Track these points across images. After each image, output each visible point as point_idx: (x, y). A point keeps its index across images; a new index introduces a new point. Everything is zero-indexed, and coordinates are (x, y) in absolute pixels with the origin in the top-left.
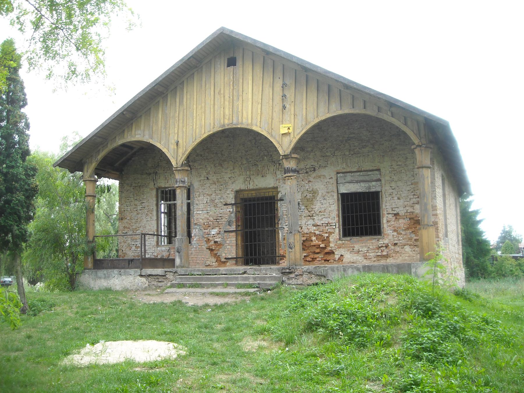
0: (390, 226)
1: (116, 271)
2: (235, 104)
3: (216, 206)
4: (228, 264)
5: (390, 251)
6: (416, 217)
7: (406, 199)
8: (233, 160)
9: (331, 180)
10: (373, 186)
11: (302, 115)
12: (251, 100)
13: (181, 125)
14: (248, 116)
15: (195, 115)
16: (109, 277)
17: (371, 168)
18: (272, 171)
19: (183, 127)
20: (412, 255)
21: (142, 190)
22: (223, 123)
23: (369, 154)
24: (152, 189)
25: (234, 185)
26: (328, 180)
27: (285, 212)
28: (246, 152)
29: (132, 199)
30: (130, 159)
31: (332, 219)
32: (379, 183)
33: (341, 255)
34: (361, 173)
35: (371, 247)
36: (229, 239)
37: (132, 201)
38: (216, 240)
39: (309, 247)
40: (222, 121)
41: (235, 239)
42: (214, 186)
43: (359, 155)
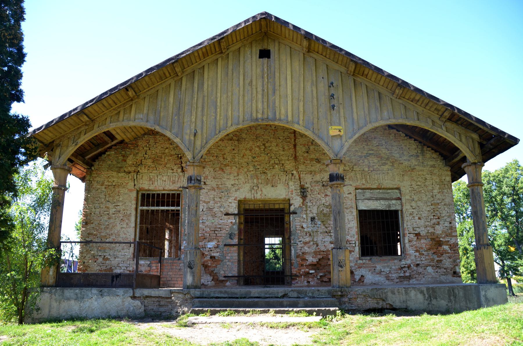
0: (412, 246)
1: (95, 291)
2: (271, 98)
3: (214, 216)
4: (228, 284)
5: (412, 272)
6: (437, 237)
7: (426, 219)
8: (237, 166)
9: (349, 195)
10: (393, 204)
11: (353, 119)
12: (290, 96)
13: (199, 113)
14: (287, 112)
15: (218, 104)
16: (83, 298)
17: (391, 186)
18: (284, 181)
19: (203, 115)
20: (435, 276)
21: (117, 190)
22: (255, 117)
23: (389, 172)
24: (131, 191)
25: (238, 193)
26: (347, 195)
27: (298, 226)
28: (254, 158)
29: (103, 200)
30: (104, 153)
31: (351, 237)
32: (399, 202)
33: (362, 276)
34: (381, 191)
35: (393, 267)
36: (229, 255)
37: (102, 203)
38: (213, 254)
39: (324, 266)
40: (254, 115)
41: (236, 254)
42: (213, 192)
43: (379, 172)
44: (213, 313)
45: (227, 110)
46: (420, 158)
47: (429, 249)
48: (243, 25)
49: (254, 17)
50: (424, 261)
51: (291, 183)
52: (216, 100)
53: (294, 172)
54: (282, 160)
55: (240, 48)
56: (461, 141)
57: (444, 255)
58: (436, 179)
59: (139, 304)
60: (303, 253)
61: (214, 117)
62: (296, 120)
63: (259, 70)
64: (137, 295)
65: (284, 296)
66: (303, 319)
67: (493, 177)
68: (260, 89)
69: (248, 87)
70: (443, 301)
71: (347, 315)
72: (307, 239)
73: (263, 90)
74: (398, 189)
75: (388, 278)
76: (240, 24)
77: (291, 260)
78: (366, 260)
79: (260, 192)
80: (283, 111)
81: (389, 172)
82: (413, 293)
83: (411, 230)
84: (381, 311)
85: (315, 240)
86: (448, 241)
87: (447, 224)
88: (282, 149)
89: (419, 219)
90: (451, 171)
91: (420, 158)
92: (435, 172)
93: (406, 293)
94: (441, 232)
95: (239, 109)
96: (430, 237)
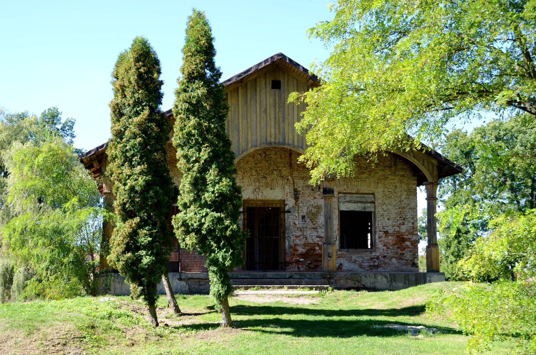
0: (381, 241)
2: (282, 125)
8: (242, 170)
15: (241, 128)
17: (367, 192)
28: (256, 164)
32: (373, 205)
33: (341, 264)
34: (359, 195)
35: (365, 258)
40: (269, 139)
44: (246, 289)
45: (247, 134)
46: (393, 169)
47: (395, 244)
48: (263, 65)
49: (272, 57)
50: (390, 253)
51: (286, 187)
52: (239, 125)
53: (290, 178)
54: (279, 167)
55: (256, 78)
56: (423, 165)
57: (406, 249)
58: (405, 187)
59: (185, 284)
60: (295, 245)
61: (237, 140)
62: (300, 145)
63: (272, 100)
64: (183, 277)
65: (289, 278)
66: (307, 292)
67: (503, 130)
68: (272, 117)
69: (263, 115)
70: (400, 284)
71: (335, 290)
72: (299, 234)
73: (275, 118)
74: (373, 194)
75: (361, 266)
76: (261, 63)
77: (285, 250)
78: (344, 252)
79: (261, 194)
80: (291, 137)
81: (367, 179)
82: (379, 277)
83: (381, 229)
84: (358, 289)
85: (305, 234)
86: (410, 238)
87: (410, 225)
88: (279, 157)
89: (388, 219)
90: (417, 180)
91: (393, 169)
92: (404, 181)
93: (375, 277)
94: (405, 231)
95: (257, 133)
96: (395, 235)
